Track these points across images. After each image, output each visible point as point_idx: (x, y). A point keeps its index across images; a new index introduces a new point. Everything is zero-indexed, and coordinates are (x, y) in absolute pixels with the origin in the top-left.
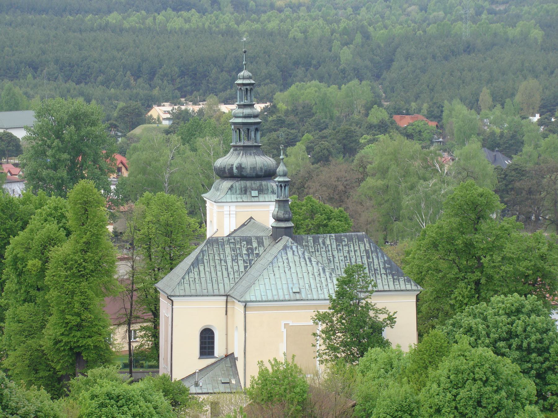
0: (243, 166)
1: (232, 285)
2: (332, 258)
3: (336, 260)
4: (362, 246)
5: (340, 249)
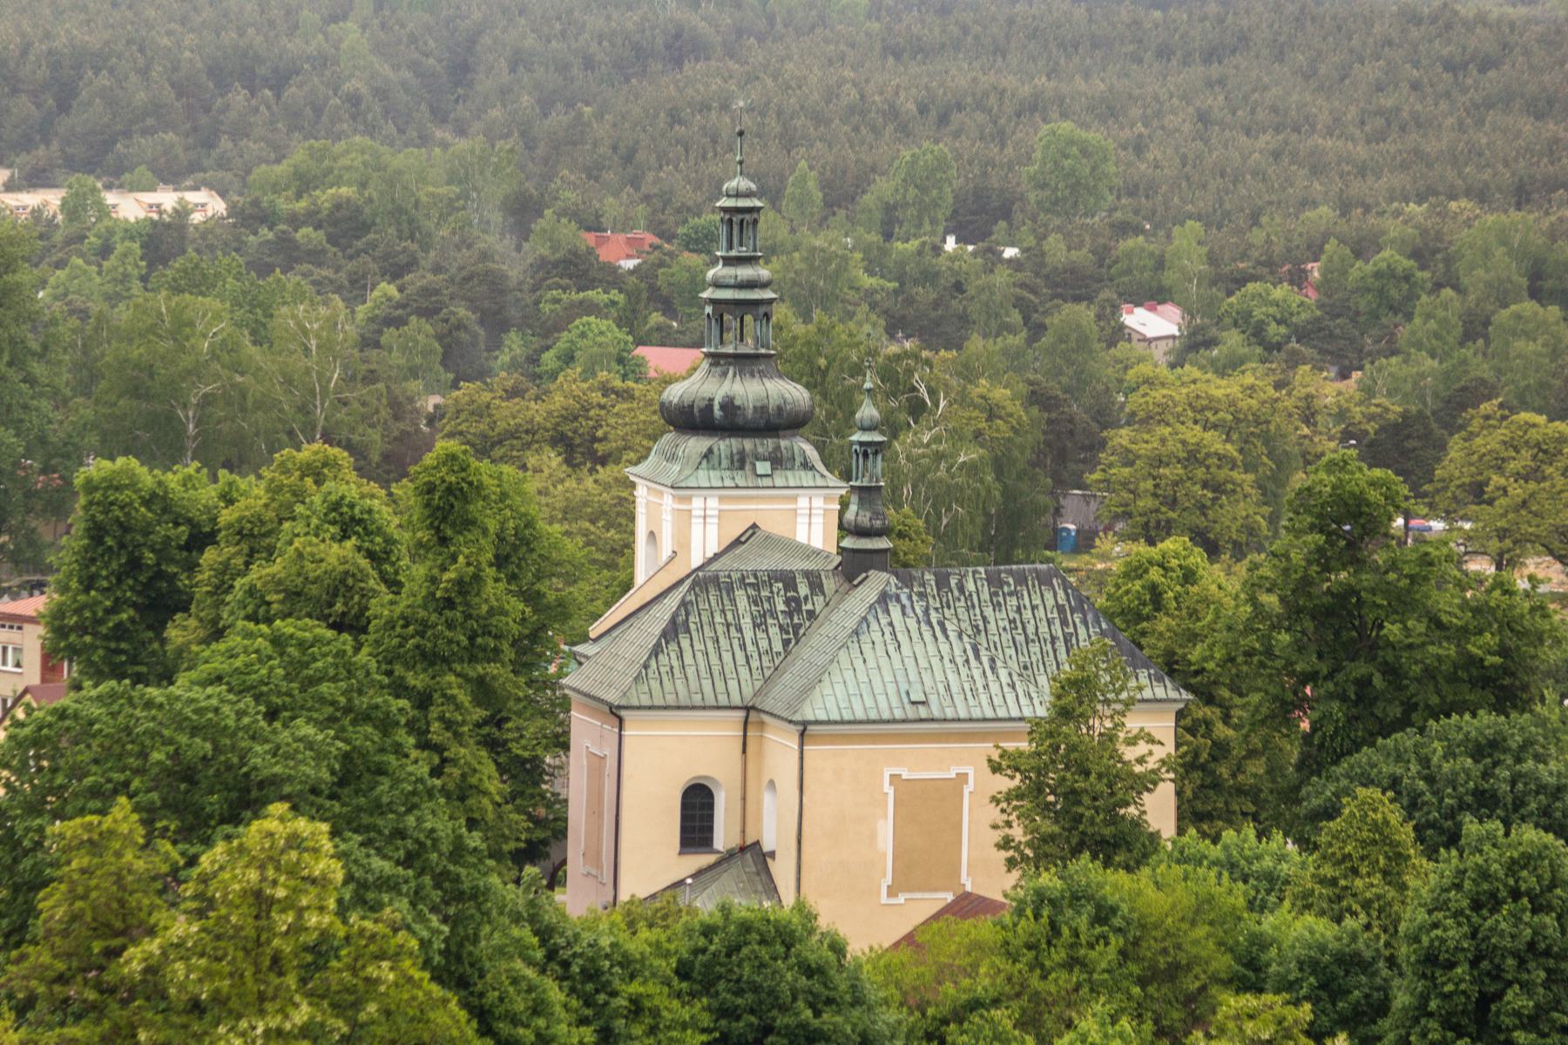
0: (737, 403)
1: (758, 684)
2: (981, 623)
3: (992, 627)
4: (1049, 596)
5: (999, 603)
